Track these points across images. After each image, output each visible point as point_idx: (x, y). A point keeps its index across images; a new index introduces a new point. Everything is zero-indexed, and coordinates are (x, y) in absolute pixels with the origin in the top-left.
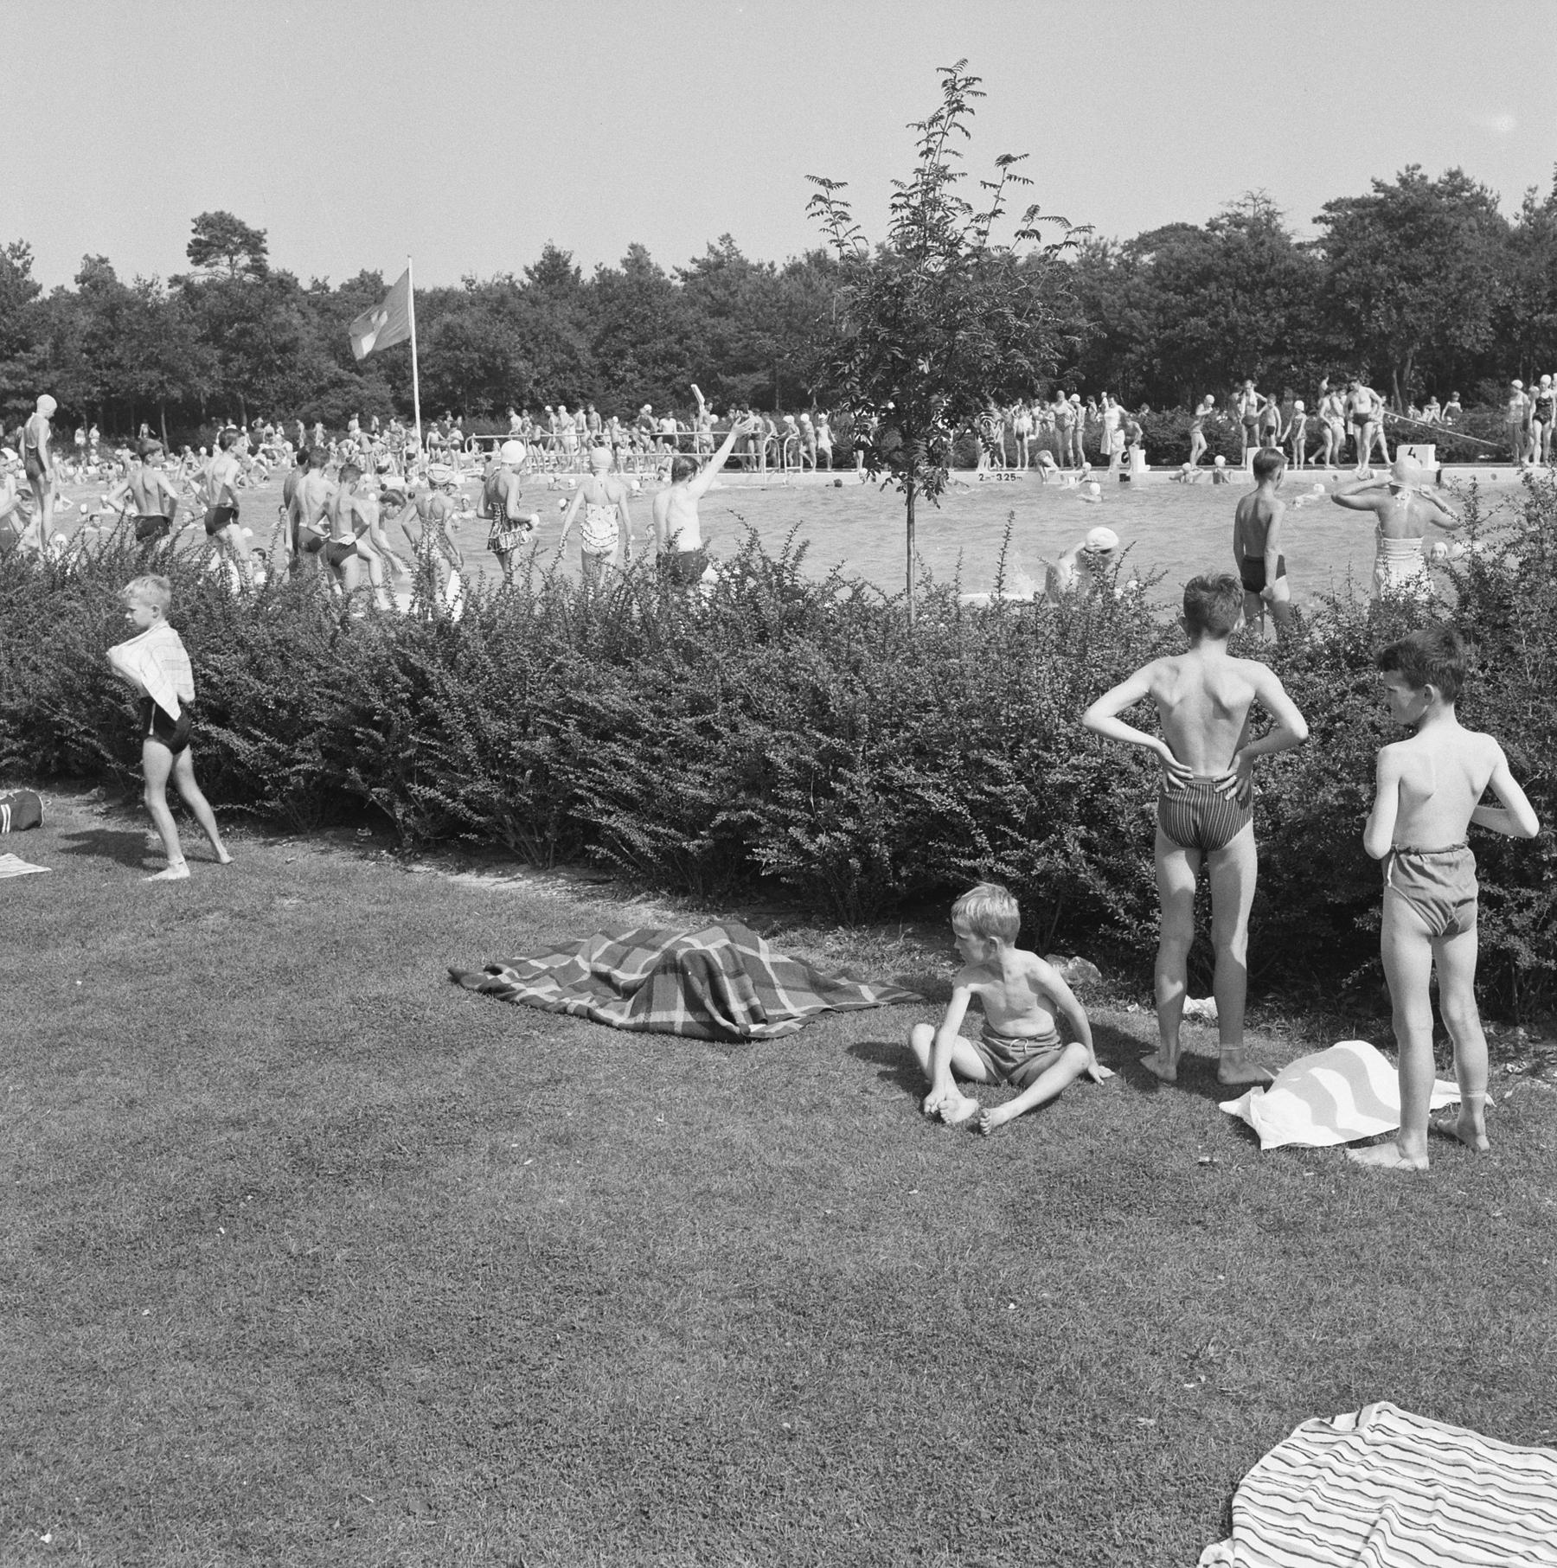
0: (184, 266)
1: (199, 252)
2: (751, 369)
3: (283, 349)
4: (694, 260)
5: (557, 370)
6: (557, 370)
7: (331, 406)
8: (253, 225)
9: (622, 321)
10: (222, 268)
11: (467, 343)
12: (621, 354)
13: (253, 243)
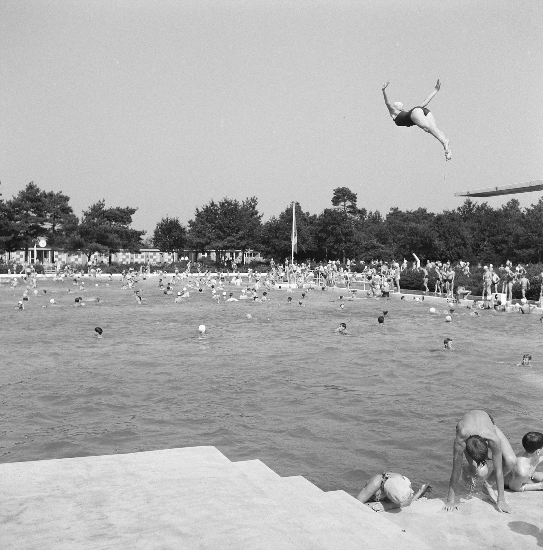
0: (330, 206)
1: (336, 201)
2: (528, 247)
3: (346, 235)
4: (532, 205)
5: (456, 245)
6: (456, 245)
7: (370, 256)
8: (353, 192)
9: (486, 228)
10: (341, 207)
11: (417, 234)
12: (484, 240)
13: (353, 198)
